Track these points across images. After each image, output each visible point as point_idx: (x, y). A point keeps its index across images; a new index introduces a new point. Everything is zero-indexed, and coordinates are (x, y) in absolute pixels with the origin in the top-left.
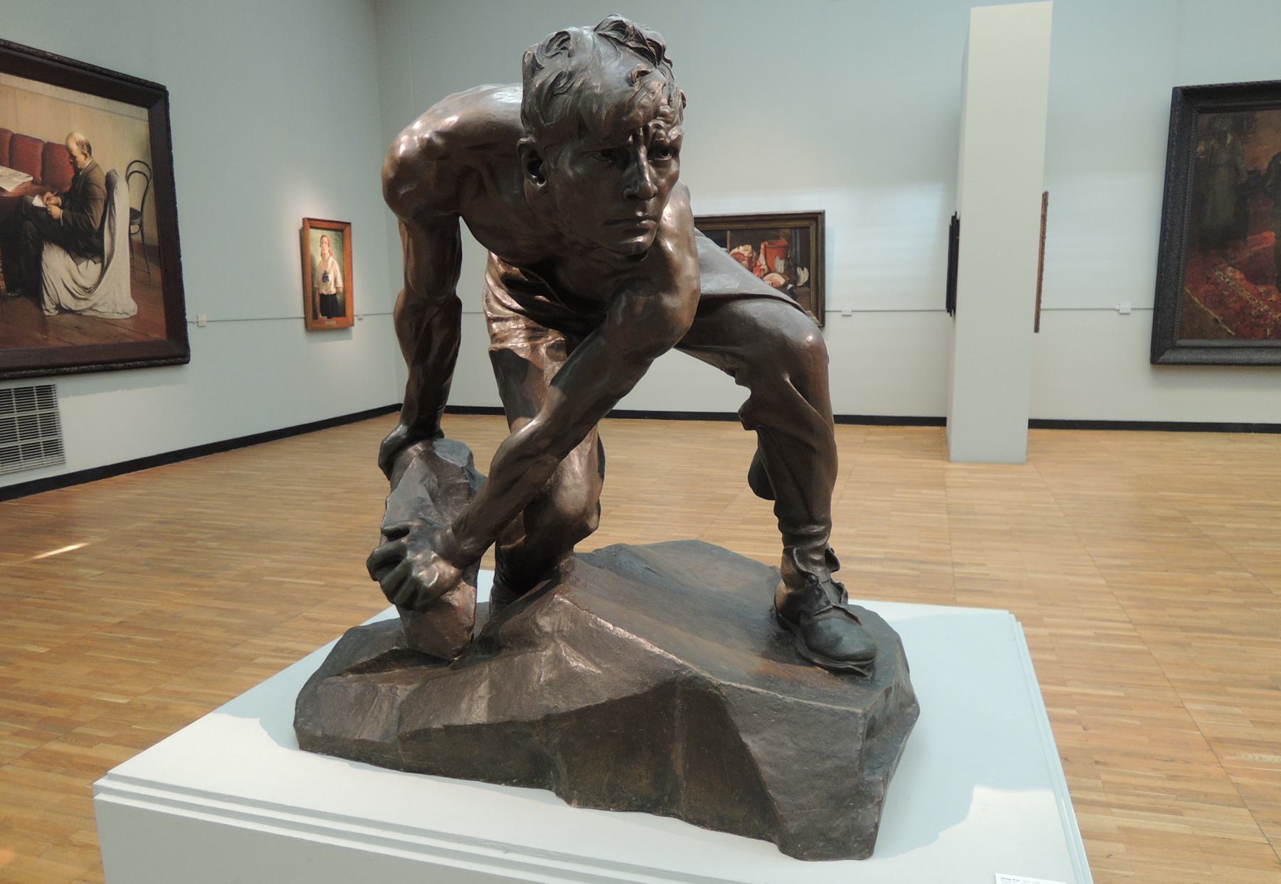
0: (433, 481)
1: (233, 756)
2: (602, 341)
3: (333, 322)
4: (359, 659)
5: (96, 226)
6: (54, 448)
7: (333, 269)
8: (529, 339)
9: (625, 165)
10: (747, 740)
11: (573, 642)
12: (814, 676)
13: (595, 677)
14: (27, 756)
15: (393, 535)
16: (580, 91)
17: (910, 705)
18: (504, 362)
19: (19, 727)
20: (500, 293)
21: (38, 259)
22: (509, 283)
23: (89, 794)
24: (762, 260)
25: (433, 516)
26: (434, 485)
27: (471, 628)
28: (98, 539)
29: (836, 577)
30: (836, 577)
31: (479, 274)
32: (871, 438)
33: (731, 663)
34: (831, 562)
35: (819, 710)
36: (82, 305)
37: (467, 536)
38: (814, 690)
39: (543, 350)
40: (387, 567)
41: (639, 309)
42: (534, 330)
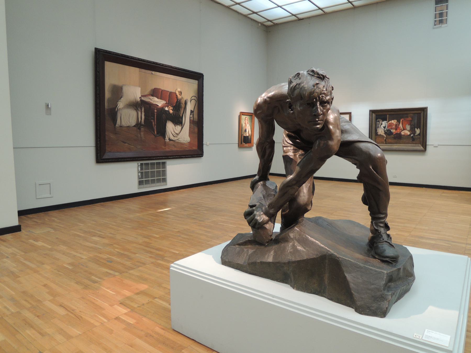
0: (264, 193)
1: (205, 264)
2: (312, 154)
3: (247, 145)
4: (240, 242)
5: (181, 116)
6: (164, 180)
7: (248, 128)
8: (294, 152)
9: (313, 107)
10: (347, 275)
11: (299, 241)
12: (376, 262)
13: (303, 251)
14: (152, 263)
15: (251, 206)
16: (301, 88)
17: (411, 277)
18: (286, 159)
19: (151, 255)
20: (287, 139)
21: (165, 125)
22: (289, 136)
23: (168, 268)
24: (401, 125)
25: (263, 202)
26: (264, 194)
27: (271, 236)
28: (174, 208)
29: (388, 232)
30: (388, 232)
31: (280, 135)
32: (444, 194)
33: (349, 256)
34: (387, 227)
35: (371, 269)
36: (175, 139)
37: (272, 208)
38: (376, 266)
39: (298, 156)
40: (249, 215)
41: (322, 145)
42: (295, 150)
